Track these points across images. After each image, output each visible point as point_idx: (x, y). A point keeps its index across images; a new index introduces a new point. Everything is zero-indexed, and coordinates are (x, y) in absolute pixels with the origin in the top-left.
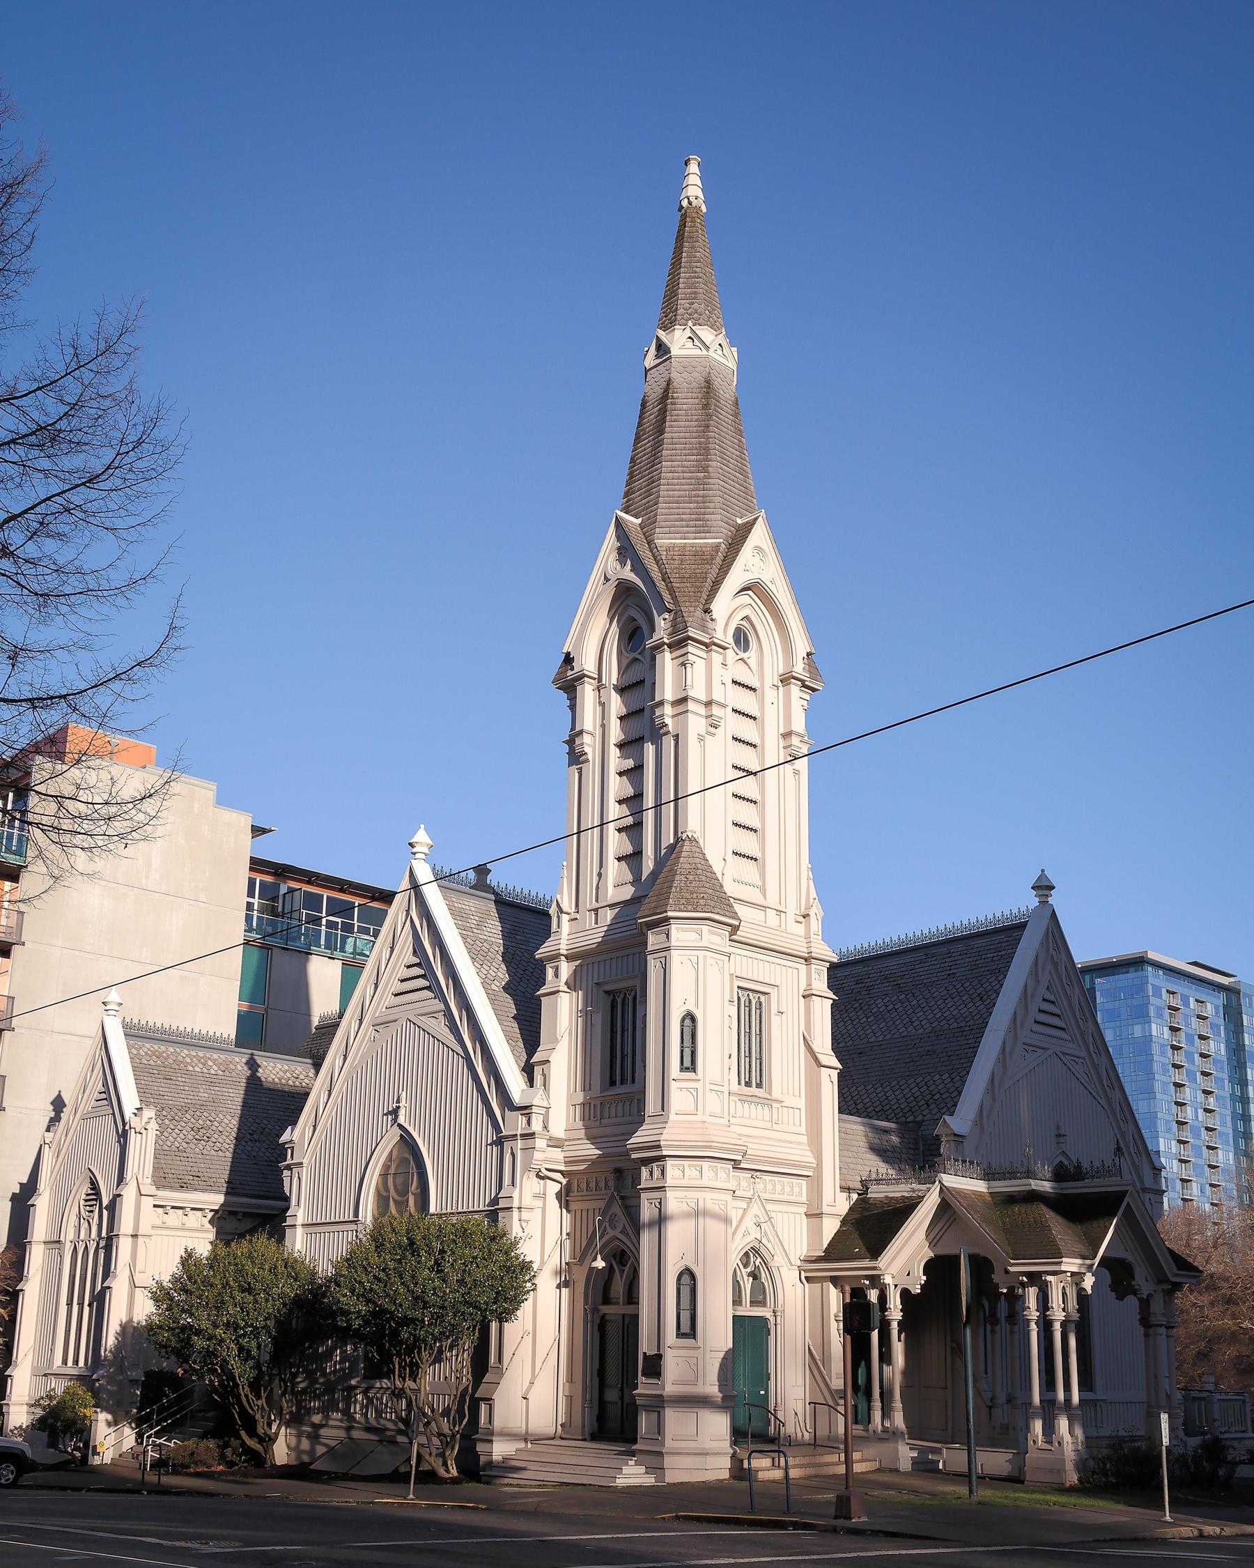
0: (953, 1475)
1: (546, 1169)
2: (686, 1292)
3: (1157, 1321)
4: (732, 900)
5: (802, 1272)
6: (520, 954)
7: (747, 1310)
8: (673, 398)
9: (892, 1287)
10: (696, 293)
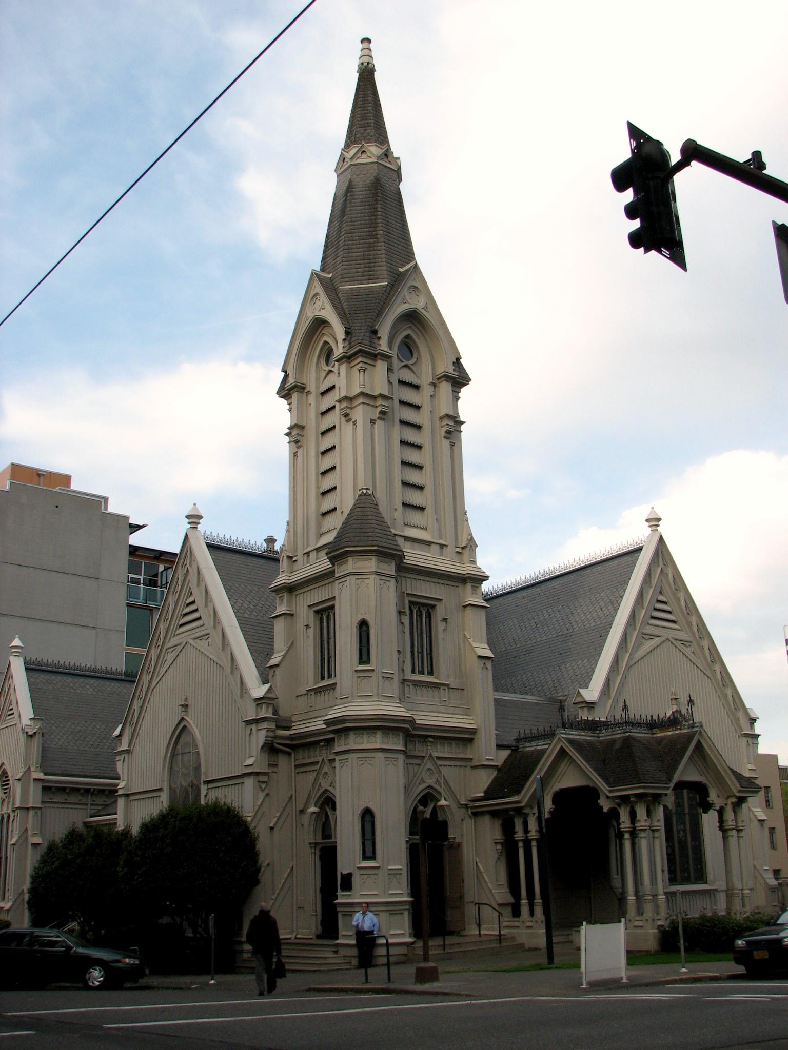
3: (654, 826)
4: (400, 541)
6: (237, 586)
8: (352, 192)
10: (368, 123)
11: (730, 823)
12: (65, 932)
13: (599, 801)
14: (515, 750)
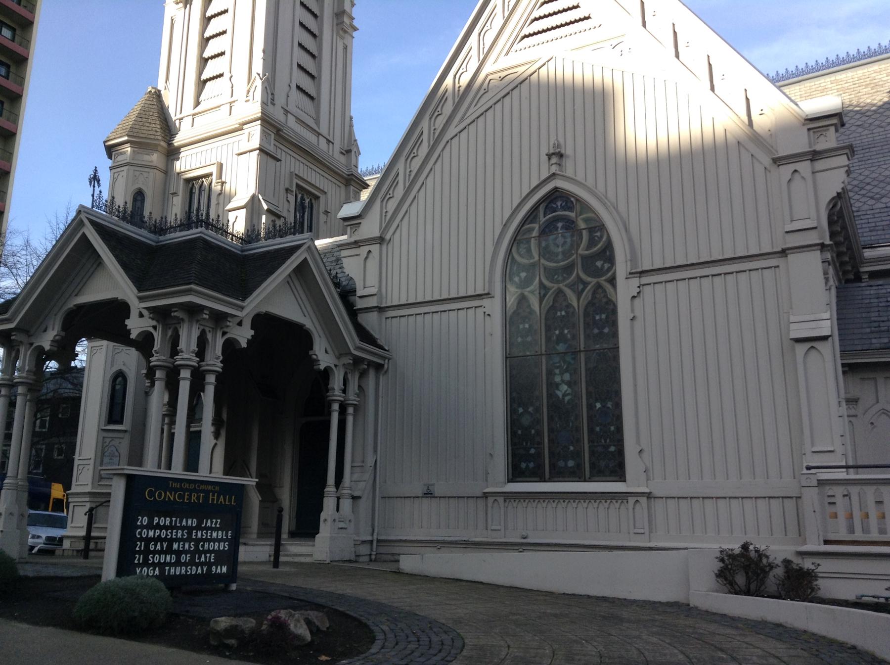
11: (336, 393)
12: (35, 554)
13: (127, 322)
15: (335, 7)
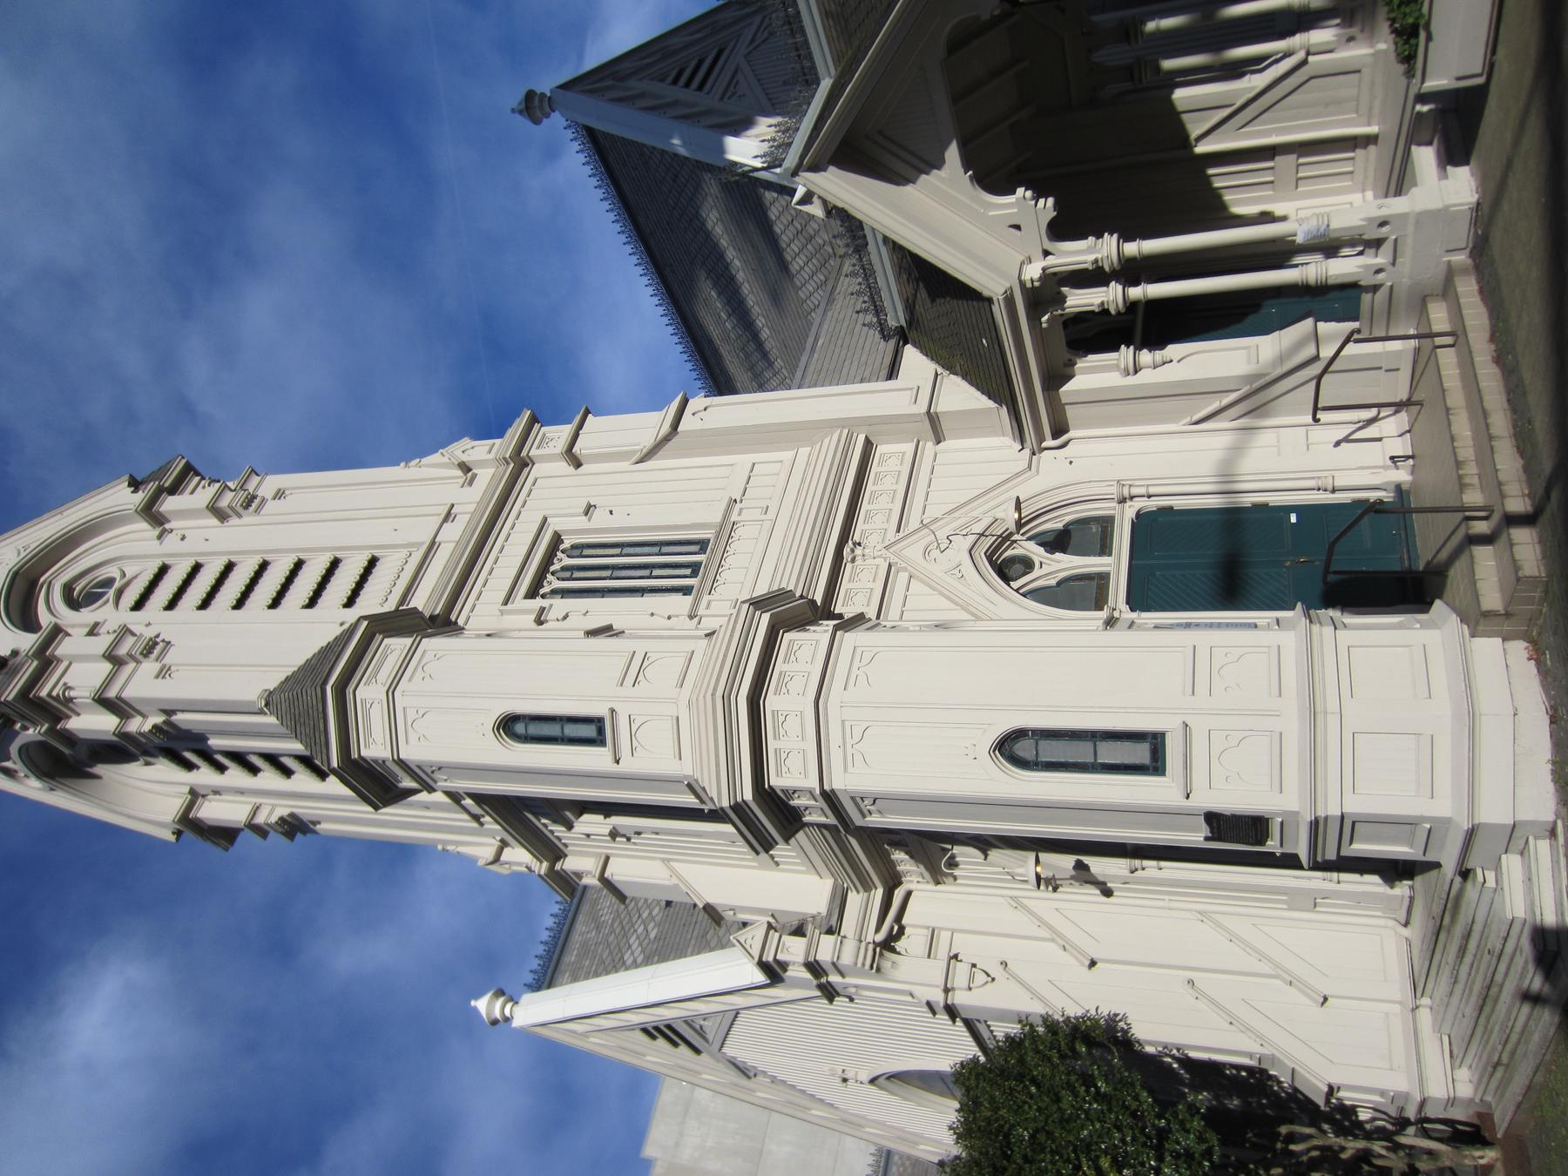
0: (1494, 52)
1: (878, 930)
2: (1050, 751)
5: (1044, 445)
7: (1116, 565)
9: (1050, 260)
14: (903, 337)
15: (82, 700)
